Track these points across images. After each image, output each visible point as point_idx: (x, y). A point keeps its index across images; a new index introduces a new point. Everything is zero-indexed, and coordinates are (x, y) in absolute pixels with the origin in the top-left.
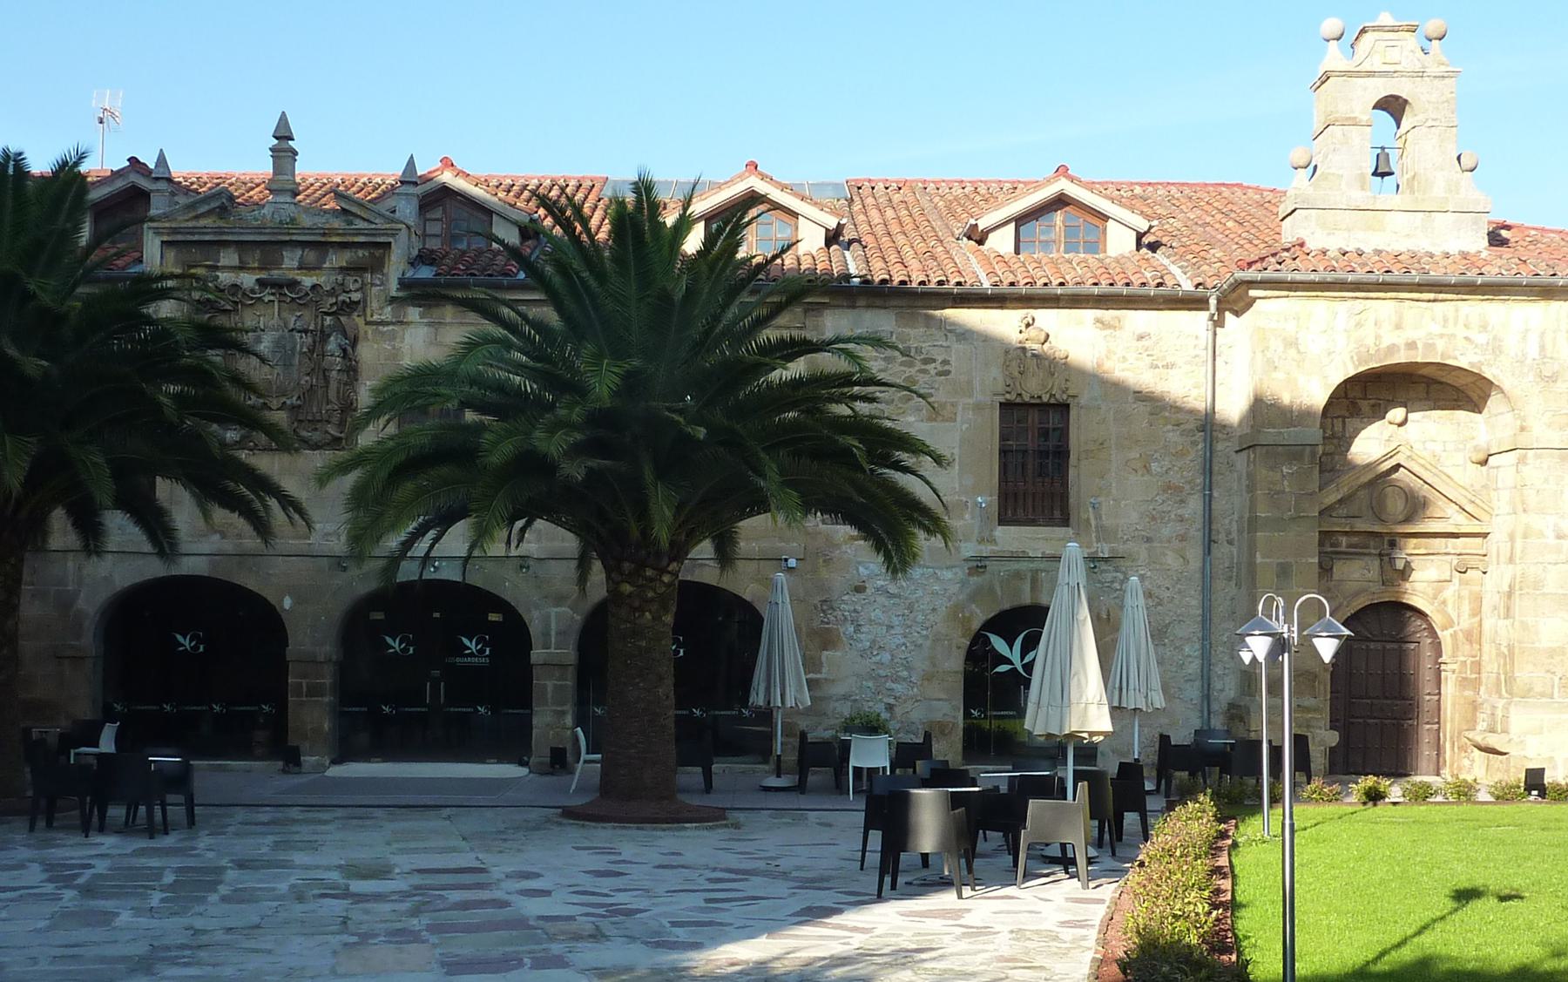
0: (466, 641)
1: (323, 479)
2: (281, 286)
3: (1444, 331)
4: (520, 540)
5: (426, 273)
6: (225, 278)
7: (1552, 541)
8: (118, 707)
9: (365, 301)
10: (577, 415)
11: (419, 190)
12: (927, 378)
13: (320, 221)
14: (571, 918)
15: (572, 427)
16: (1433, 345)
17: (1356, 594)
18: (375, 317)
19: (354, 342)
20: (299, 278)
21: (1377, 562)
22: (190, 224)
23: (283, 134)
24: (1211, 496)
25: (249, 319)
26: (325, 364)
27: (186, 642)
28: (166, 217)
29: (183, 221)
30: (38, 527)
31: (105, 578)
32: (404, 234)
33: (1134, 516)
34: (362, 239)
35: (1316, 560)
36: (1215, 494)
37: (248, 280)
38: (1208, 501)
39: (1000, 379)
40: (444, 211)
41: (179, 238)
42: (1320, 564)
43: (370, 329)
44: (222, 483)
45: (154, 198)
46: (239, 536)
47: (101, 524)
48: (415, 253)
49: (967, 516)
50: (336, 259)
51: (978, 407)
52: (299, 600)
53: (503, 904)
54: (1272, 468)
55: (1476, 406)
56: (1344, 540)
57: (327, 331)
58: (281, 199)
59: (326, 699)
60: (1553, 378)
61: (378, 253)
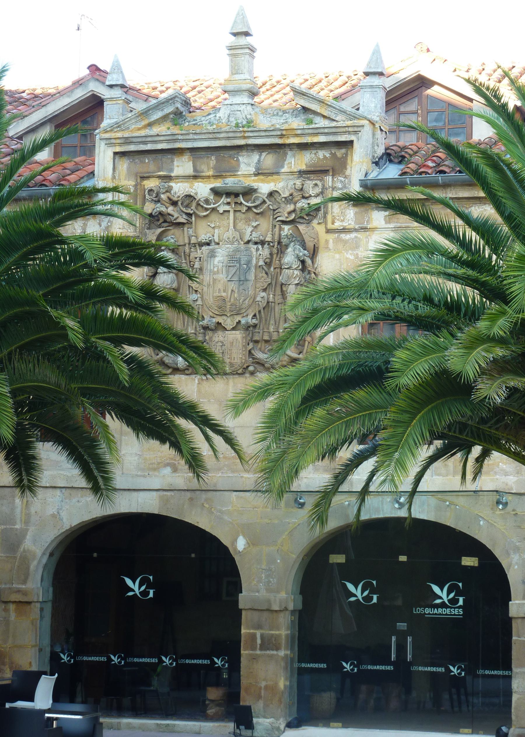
0: (436, 589)
1: (238, 407)
2: (237, 195)
4: (477, 473)
5: (392, 172)
6: (179, 189)
8: (65, 658)
10: (501, 327)
11: (389, 83)
13: (278, 122)
15: (501, 341)
18: (338, 225)
19: (314, 253)
20: (255, 185)
22: (143, 133)
25: (203, 231)
26: (282, 279)
27: (135, 587)
28: (118, 126)
29: (136, 130)
31: (53, 516)
32: (367, 129)
34: (322, 139)
37: (202, 190)
40: (420, 103)
41: (132, 148)
43: (331, 237)
44: (156, 416)
45: (108, 107)
47: (34, 457)
48: (381, 151)
50: (297, 162)
52: (252, 542)
57: (284, 241)
58: (237, 99)
59: (282, 653)
61: (340, 152)
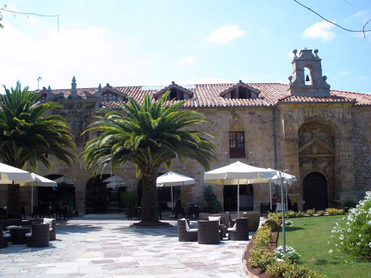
7: (348, 157)
9: (90, 114)
12: (213, 126)
14: (133, 246)
16: (320, 116)
17: (308, 171)
21: (312, 164)
23: (74, 80)
24: (276, 150)
30: (47, 160)
33: (260, 155)
35: (298, 163)
36: (277, 150)
38: (275, 151)
39: (229, 126)
46: (65, 165)
49: (223, 156)
51: (224, 132)
53: (119, 244)
54: (288, 144)
55: (46, 166)
57: (83, 121)
59: (84, 200)
60: (346, 123)
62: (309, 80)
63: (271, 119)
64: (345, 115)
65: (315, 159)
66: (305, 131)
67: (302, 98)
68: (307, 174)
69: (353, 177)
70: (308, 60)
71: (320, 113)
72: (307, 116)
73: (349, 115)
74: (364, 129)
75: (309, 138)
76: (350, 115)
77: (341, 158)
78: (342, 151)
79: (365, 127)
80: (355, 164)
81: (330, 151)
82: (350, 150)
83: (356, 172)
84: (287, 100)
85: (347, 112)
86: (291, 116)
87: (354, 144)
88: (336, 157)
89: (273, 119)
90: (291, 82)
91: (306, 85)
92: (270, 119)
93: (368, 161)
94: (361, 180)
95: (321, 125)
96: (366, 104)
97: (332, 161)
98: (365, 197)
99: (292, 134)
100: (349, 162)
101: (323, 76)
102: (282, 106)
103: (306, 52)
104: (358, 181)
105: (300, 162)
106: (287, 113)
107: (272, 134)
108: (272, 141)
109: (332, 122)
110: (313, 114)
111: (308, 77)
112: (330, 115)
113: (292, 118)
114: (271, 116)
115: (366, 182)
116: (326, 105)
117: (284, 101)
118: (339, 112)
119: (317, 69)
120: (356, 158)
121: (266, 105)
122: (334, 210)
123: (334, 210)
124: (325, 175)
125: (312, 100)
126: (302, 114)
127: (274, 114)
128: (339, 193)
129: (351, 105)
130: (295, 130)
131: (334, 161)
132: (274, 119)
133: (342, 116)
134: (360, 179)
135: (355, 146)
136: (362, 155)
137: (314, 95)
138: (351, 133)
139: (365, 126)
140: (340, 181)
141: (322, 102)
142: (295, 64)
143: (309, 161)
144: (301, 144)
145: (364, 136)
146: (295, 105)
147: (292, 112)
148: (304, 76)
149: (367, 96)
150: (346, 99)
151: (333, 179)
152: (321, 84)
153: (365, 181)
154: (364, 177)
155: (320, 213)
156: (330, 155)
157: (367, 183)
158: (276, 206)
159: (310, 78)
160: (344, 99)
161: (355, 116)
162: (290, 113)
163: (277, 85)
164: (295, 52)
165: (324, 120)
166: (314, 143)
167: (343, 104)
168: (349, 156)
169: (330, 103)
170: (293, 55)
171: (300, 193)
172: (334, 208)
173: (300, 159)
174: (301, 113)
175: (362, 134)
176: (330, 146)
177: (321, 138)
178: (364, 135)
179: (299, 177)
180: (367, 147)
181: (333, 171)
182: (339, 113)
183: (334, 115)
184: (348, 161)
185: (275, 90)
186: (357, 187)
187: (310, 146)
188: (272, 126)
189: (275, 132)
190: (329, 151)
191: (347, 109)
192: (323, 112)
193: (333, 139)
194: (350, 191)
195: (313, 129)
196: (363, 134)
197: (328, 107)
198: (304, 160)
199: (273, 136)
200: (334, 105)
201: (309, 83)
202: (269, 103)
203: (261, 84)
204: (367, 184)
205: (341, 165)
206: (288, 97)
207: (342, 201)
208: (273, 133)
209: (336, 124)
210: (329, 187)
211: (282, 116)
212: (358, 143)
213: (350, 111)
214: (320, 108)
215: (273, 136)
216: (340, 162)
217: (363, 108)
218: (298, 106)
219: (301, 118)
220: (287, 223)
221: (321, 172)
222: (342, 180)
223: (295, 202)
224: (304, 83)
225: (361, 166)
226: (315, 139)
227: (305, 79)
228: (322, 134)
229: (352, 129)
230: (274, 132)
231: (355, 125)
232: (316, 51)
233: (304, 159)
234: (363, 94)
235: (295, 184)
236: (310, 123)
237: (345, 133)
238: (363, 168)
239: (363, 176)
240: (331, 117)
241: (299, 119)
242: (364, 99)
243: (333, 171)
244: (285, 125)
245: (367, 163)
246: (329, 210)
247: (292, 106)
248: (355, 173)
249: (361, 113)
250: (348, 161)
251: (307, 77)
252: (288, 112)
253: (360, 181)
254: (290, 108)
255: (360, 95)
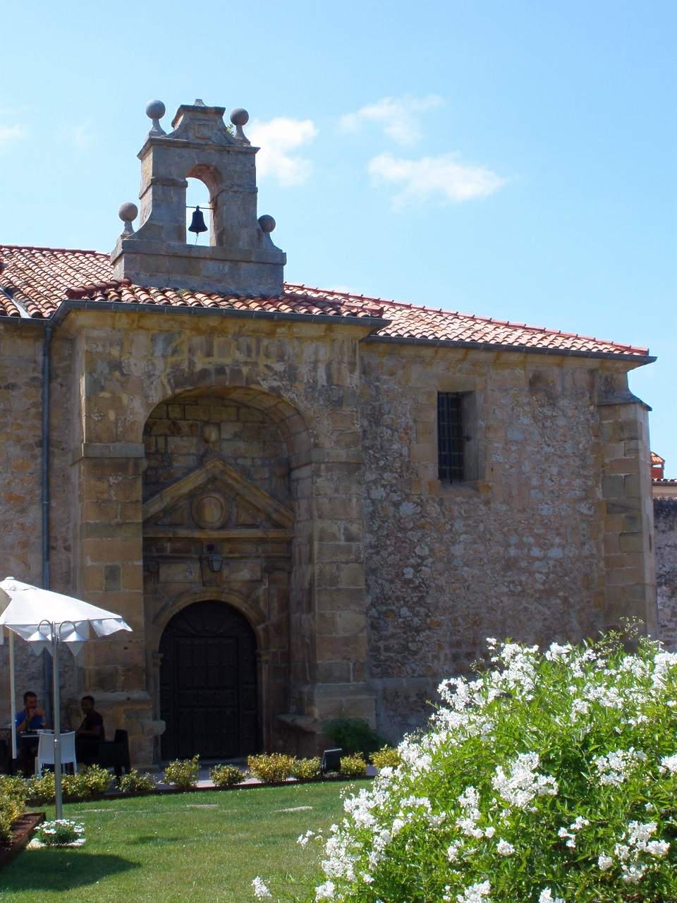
3: (249, 360)
7: (343, 543)
16: (239, 372)
17: (181, 594)
21: (197, 566)
35: (140, 563)
36: (53, 504)
38: (47, 510)
42: (144, 566)
54: (99, 479)
56: (168, 546)
60: (339, 402)
62: (204, 229)
63: (36, 375)
64: (339, 370)
65: (211, 548)
66: (175, 430)
67: (168, 294)
68: (176, 610)
69: (362, 620)
70: (202, 147)
71: (240, 356)
72: (185, 366)
73: (352, 371)
74: (407, 434)
75: (191, 461)
76: (357, 373)
77: (316, 545)
78: (320, 517)
79: (411, 429)
80: (373, 571)
81: (275, 516)
82: (354, 513)
83: (373, 605)
84: (106, 296)
85: (346, 359)
86: (116, 366)
87: (369, 494)
88: (300, 539)
89: (43, 373)
90: (129, 228)
91: (191, 247)
92: (31, 375)
93: (419, 561)
94: (393, 636)
95: (243, 410)
96: (418, 336)
97: (281, 558)
98: (433, 717)
99: (116, 439)
100: (347, 563)
101: (258, 218)
102: (82, 319)
103: (201, 116)
104: (380, 639)
105: (145, 559)
106: (100, 349)
107: (37, 439)
108: (36, 465)
109: (286, 396)
110: (210, 359)
111: (201, 213)
112: (279, 367)
113: (123, 374)
114: (35, 362)
115: (410, 644)
116: (264, 325)
117: (94, 299)
118: (313, 359)
119: (239, 186)
120: (376, 548)
121: (18, 314)
122: (280, 764)
123: (282, 761)
124: (251, 615)
125: (207, 303)
126: (164, 356)
127: (48, 352)
128: (306, 689)
129: (361, 333)
130: (133, 423)
131: (289, 559)
132: (50, 375)
133: (324, 377)
134: (388, 633)
135: (373, 502)
136: (400, 535)
137: (220, 287)
138: (360, 447)
139: (411, 423)
140: (312, 638)
141: (248, 314)
142: (150, 158)
143: (187, 555)
144: (153, 484)
145: (409, 462)
146: (136, 317)
147: (122, 345)
148: (182, 207)
149: (423, 315)
150: (343, 309)
151: (284, 628)
152: (250, 245)
153: (408, 642)
154: (404, 623)
155: (222, 774)
156: (273, 534)
157: (415, 649)
158: (35, 741)
159: (208, 219)
160: (338, 309)
161: (378, 380)
162: (115, 352)
163: (81, 258)
164: (156, 111)
165: (253, 386)
166: (213, 479)
167: (333, 326)
168: (350, 538)
169: (279, 318)
170: (148, 124)
171: (147, 688)
172: (284, 751)
173: (150, 545)
174: (158, 353)
175: (401, 455)
176: (273, 496)
177: (240, 461)
178: (409, 456)
179: (141, 619)
180: (418, 504)
181: (285, 605)
182: (316, 362)
183: (296, 369)
184: (343, 558)
185: (70, 271)
186: (375, 663)
187: (191, 495)
188: (34, 405)
189: (48, 429)
190: (269, 518)
191: (345, 350)
192: (249, 356)
193: (287, 471)
194: (348, 680)
195: (207, 423)
196: (405, 451)
197: (271, 334)
198: (169, 548)
199: (40, 444)
200: (295, 330)
201: (205, 239)
202: (33, 306)
203: (20, 249)
204: (416, 653)
205: (317, 572)
206: (109, 286)
207: (316, 720)
208: (39, 433)
209: (303, 405)
210: (267, 662)
211: (81, 364)
212: (384, 486)
213: (357, 357)
214: (238, 335)
215: (40, 444)
216: (310, 560)
217: (408, 352)
218: (151, 321)
219: (157, 373)
220: (52, 831)
221: (235, 601)
222: (317, 635)
223: (123, 728)
224: (182, 237)
225: (392, 582)
226: (214, 465)
227: (189, 221)
228: (241, 445)
229: (365, 431)
230: (43, 432)
231: (375, 417)
232: (240, 118)
233: (168, 546)
234: (409, 307)
235: (126, 648)
236: (196, 401)
237: (337, 442)
238: (399, 587)
239: (401, 620)
240: (281, 376)
241: (150, 376)
242: (412, 322)
243: (285, 605)
244: (88, 399)
245: (417, 568)
246: (263, 762)
247: (123, 321)
248: (368, 609)
249: (400, 372)
250: (343, 558)
251: (198, 216)
252: (104, 346)
253: (387, 638)
254: (114, 328)
255: (398, 308)
